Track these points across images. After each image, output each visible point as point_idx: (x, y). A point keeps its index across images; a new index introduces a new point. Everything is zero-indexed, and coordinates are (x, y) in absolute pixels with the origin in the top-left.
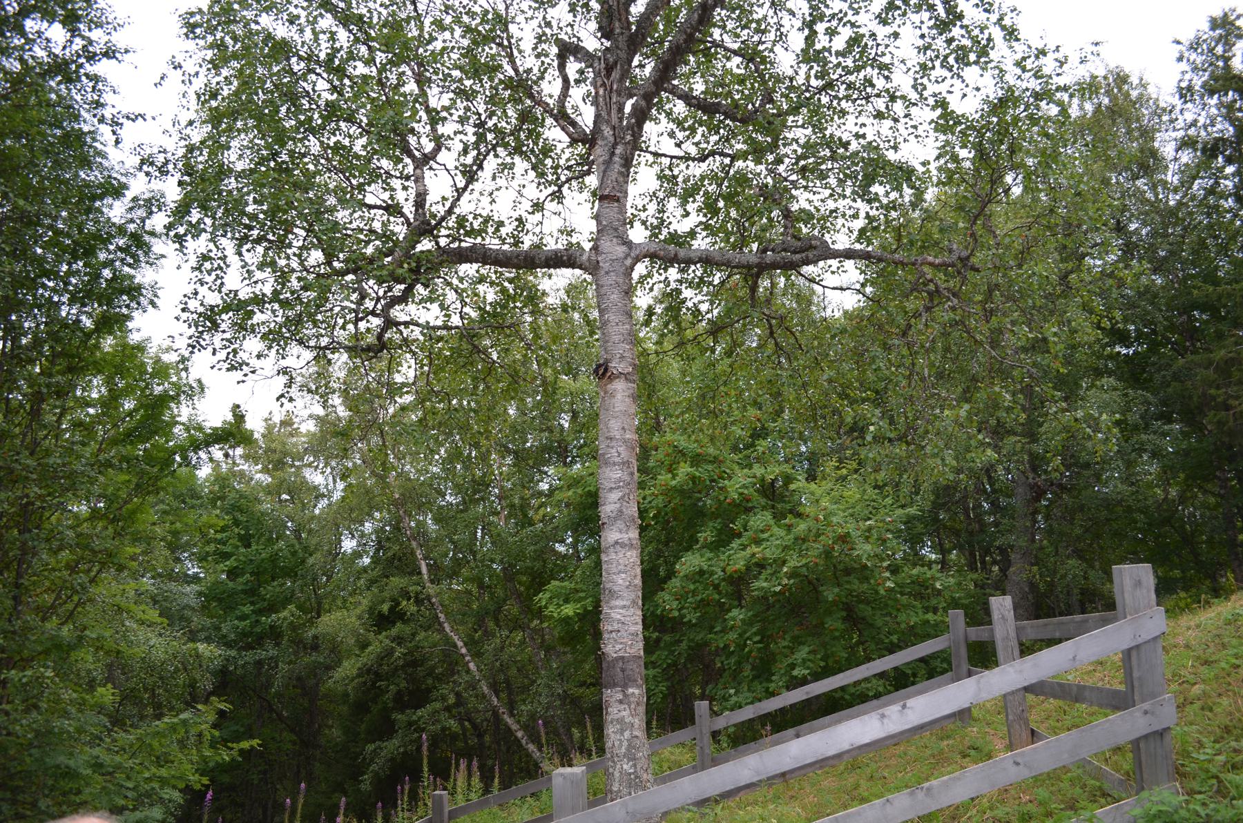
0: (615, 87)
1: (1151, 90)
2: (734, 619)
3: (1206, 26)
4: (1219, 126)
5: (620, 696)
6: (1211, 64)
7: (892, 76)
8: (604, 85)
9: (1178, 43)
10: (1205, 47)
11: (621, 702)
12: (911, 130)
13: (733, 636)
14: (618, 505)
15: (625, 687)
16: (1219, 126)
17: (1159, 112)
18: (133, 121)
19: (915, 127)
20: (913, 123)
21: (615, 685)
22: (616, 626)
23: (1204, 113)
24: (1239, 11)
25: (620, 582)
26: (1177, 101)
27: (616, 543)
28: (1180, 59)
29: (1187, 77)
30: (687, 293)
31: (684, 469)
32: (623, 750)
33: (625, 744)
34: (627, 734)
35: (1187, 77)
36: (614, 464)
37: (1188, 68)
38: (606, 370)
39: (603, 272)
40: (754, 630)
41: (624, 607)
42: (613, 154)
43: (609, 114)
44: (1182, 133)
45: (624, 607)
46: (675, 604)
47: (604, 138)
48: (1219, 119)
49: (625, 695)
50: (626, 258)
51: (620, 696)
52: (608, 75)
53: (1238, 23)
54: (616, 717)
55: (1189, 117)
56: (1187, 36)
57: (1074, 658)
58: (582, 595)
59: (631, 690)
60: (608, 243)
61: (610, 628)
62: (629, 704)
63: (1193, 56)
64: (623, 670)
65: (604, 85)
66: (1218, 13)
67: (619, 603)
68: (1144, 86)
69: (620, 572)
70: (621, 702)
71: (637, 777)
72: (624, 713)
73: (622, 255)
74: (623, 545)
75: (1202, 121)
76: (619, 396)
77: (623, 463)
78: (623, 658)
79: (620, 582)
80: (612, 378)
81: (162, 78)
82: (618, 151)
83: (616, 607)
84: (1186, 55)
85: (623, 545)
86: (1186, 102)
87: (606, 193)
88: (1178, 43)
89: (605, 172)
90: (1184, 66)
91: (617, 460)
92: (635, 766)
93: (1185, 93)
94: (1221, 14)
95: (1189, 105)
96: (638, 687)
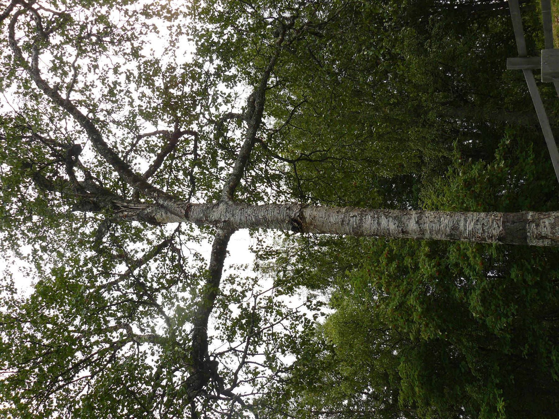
0: (126, 204)
2: (517, 276)
11: (538, 225)
13: (529, 278)
14: (391, 219)
21: (524, 229)
22: (479, 226)
25: (446, 221)
27: (417, 222)
30: (213, 35)
31: (411, 300)
36: (361, 220)
39: (232, 219)
40: (526, 263)
41: (466, 220)
42: (162, 206)
43: (139, 209)
45: (466, 220)
46: (504, 320)
49: (533, 221)
54: (549, 229)
58: (491, 395)
59: (529, 217)
60: (215, 214)
61: (481, 231)
62: (540, 219)
64: (513, 222)
67: (462, 224)
70: (538, 225)
72: (547, 223)
76: (315, 213)
77: (361, 214)
78: (504, 223)
79: (446, 221)
80: (302, 216)
83: (465, 225)
87: (184, 212)
89: (172, 213)
91: (358, 218)
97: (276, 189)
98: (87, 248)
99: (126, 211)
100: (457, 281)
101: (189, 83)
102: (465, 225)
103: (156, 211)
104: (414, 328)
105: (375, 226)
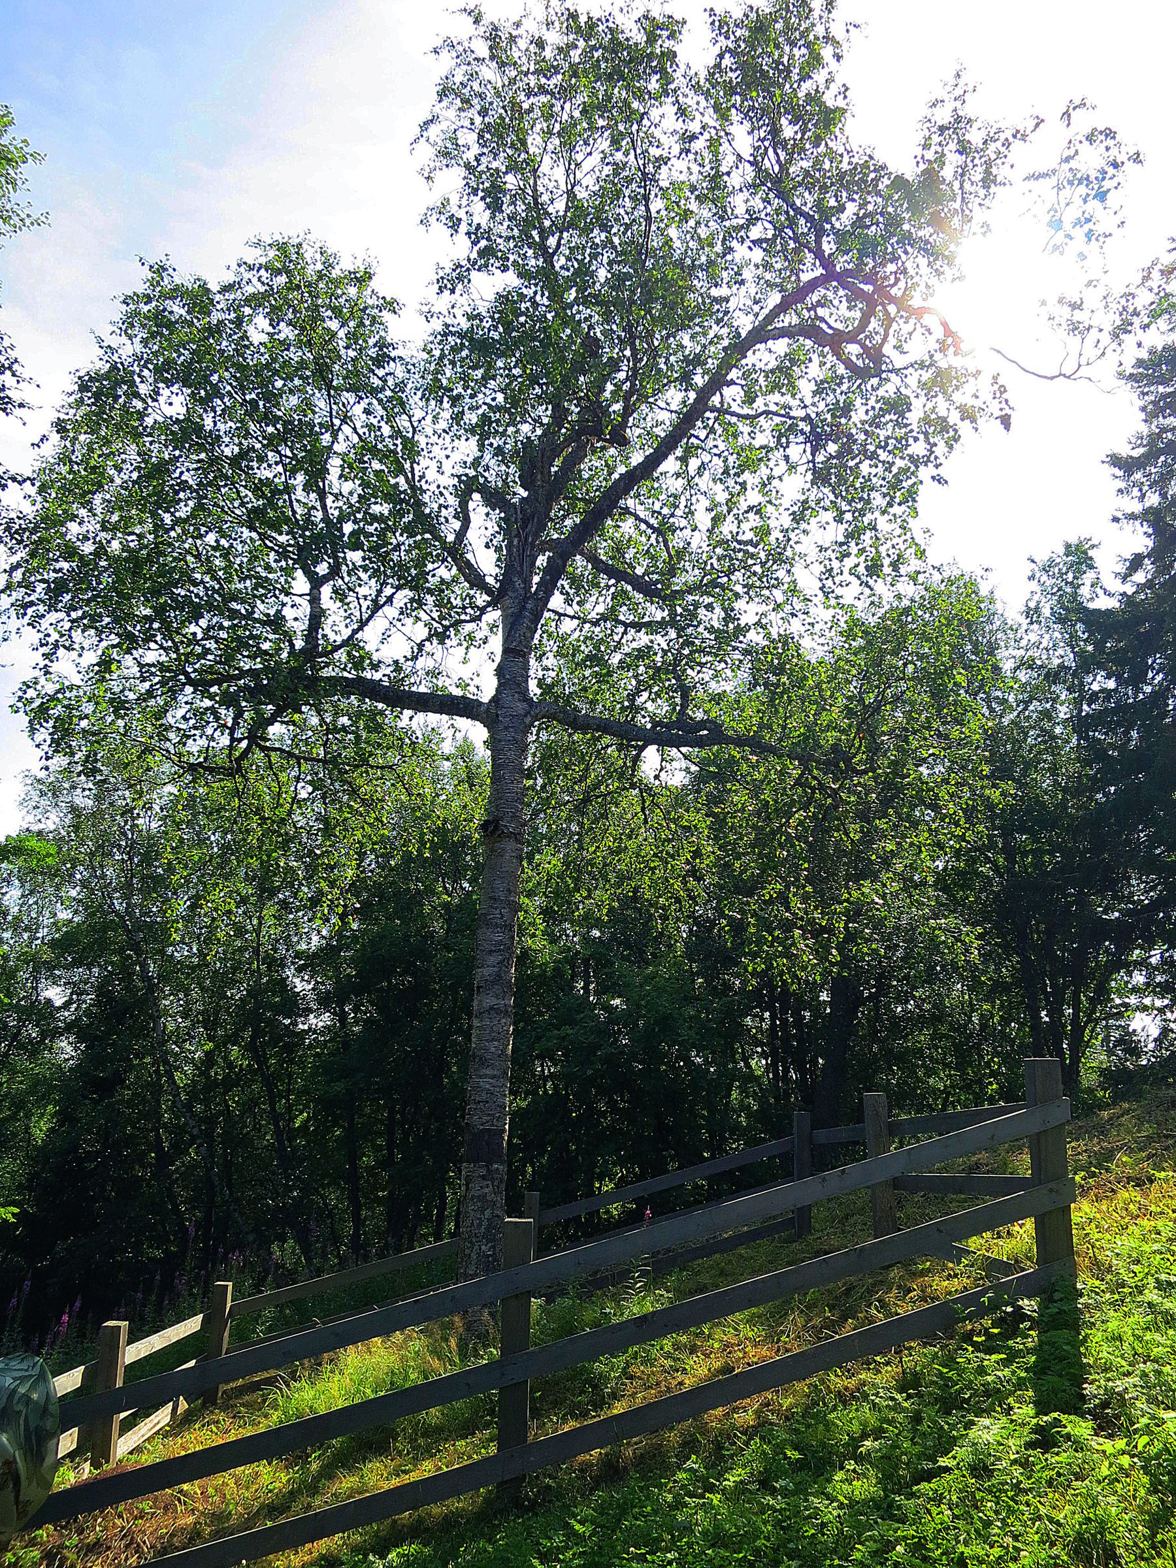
1: (999, 606)
3: (1061, 550)
4: (1060, 652)
5: (483, 1172)
6: (1060, 589)
7: (793, 570)
8: (518, 535)
9: (1033, 561)
10: (1056, 570)
11: (484, 1178)
12: (808, 627)
14: (496, 969)
15: (489, 1162)
16: (1060, 652)
17: (1005, 628)
18: (20, 483)
19: (812, 625)
20: (811, 621)
22: (484, 1096)
23: (1047, 636)
24: (1095, 541)
25: (493, 1050)
26: (1025, 622)
27: (492, 1008)
28: (1031, 578)
29: (1036, 598)
32: (483, 1230)
33: (485, 1223)
34: (487, 1213)
35: (1036, 598)
36: (497, 926)
37: (1038, 589)
38: (496, 828)
43: (522, 566)
44: (1022, 652)
47: (515, 590)
48: (1062, 644)
49: (488, 1171)
50: (526, 716)
51: (483, 1172)
52: (524, 527)
53: (1091, 553)
55: (1033, 637)
56: (1042, 557)
57: (993, 1136)
63: (1044, 578)
65: (518, 535)
66: (1073, 540)
68: (992, 601)
69: (493, 1039)
70: (484, 1178)
71: (495, 1260)
72: (486, 1190)
73: (522, 712)
74: (498, 1011)
75: (1044, 644)
79: (493, 1050)
81: (42, 440)
82: (529, 606)
83: (486, 1076)
84: (1037, 575)
85: (498, 1011)
86: (1032, 623)
88: (1033, 561)
90: (1034, 586)
92: (494, 1247)
93: (1032, 613)
94: (1076, 542)
95: (1035, 627)
96: (502, 1163)
97: (705, 581)
98: (281, 1311)
99: (519, 541)
100: (175, 449)
101: (886, 182)
102: (486, 1076)
103: (516, 597)
104: (255, 280)
105: (487, 946)
